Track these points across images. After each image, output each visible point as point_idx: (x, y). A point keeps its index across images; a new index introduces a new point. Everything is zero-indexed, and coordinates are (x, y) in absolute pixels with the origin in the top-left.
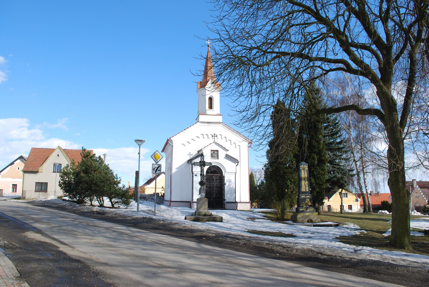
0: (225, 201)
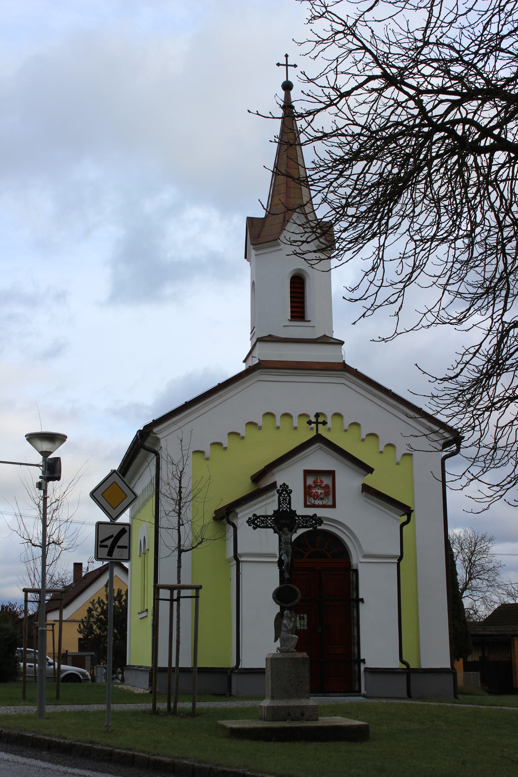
0: (363, 667)
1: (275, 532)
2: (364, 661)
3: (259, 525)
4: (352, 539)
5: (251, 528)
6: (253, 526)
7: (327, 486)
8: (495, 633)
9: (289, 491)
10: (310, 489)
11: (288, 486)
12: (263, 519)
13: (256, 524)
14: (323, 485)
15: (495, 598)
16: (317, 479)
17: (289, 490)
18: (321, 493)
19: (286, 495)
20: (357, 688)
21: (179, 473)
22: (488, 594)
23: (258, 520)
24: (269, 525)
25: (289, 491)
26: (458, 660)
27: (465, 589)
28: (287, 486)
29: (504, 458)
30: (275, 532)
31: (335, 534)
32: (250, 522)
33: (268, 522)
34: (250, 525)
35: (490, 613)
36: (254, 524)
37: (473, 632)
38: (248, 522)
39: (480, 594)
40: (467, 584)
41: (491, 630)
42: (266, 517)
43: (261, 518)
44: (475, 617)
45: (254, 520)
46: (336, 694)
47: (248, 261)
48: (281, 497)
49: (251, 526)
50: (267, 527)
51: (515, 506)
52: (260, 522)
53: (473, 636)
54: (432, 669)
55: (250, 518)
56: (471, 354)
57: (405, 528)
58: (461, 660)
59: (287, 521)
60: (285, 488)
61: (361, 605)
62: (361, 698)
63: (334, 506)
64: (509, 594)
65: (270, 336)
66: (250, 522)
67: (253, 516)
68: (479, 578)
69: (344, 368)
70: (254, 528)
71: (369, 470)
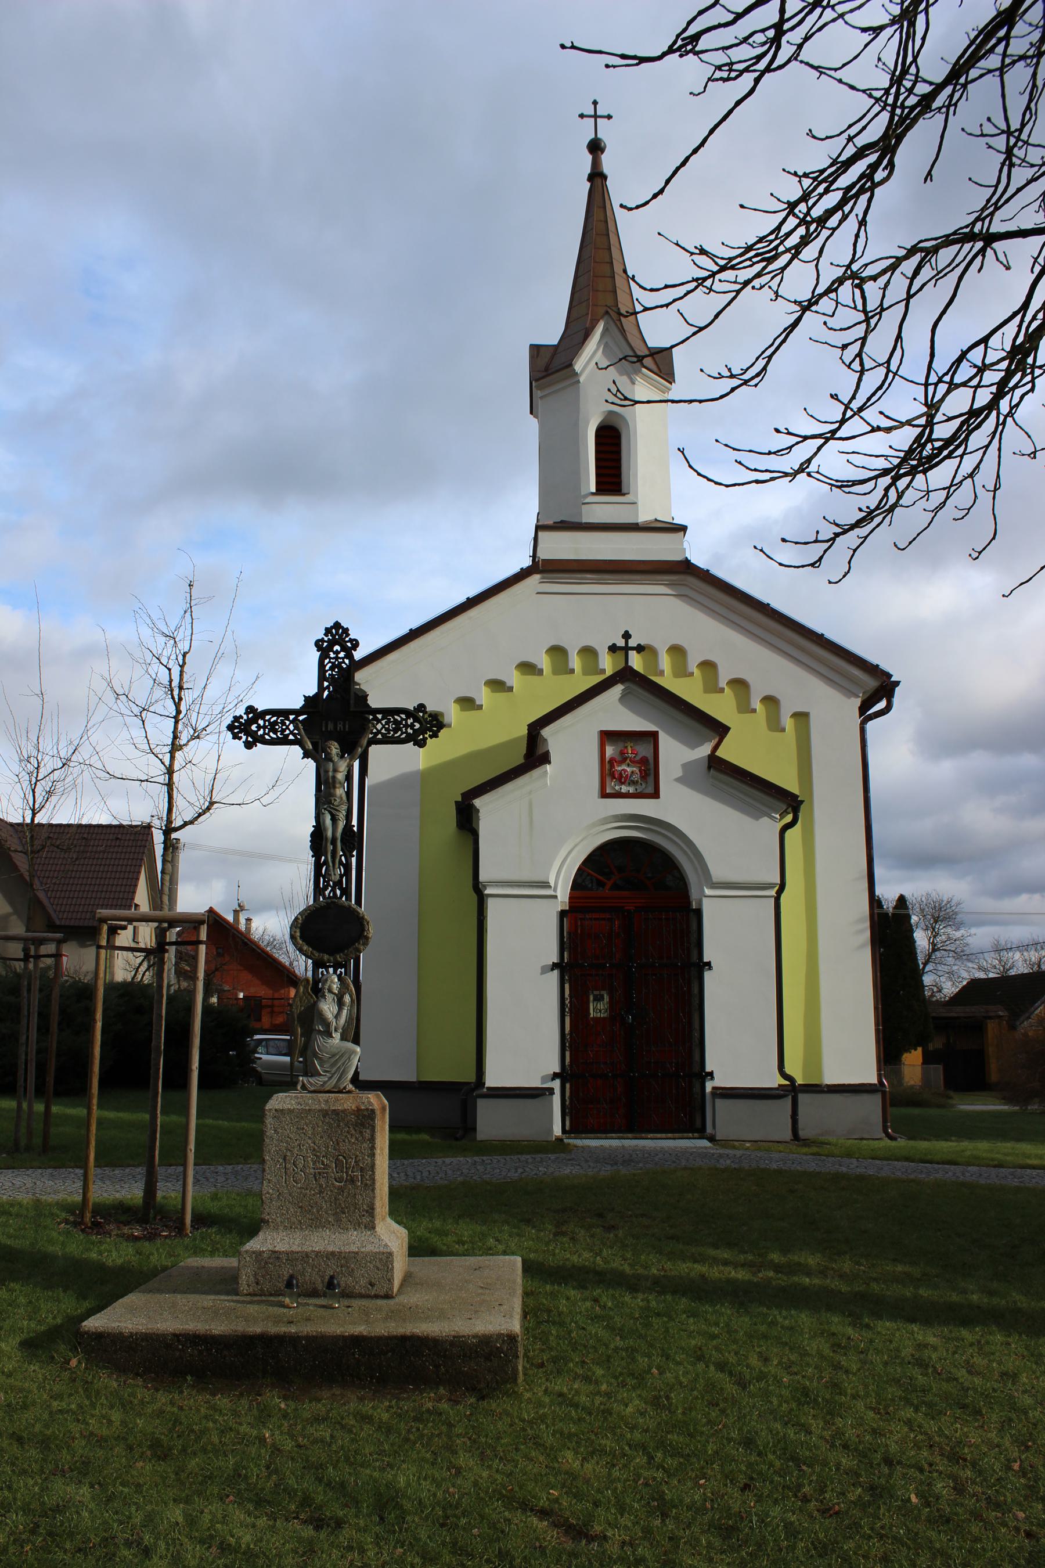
0: (709, 1086)
1: (306, 755)
2: (711, 1074)
3: (262, 736)
4: (689, 853)
5: (239, 744)
6: (244, 738)
7: (644, 761)
8: (962, 1015)
9: (349, 644)
10: (612, 766)
11: (347, 629)
12: (275, 718)
13: (253, 734)
14: (638, 758)
15: (965, 975)
16: (626, 747)
17: (351, 641)
18: (632, 772)
19: (342, 655)
20: (698, 1123)
21: (180, 658)
22: (955, 968)
23: (261, 722)
24: (291, 737)
25: (349, 644)
26: (916, 1050)
27: (925, 964)
28: (346, 631)
29: (961, 482)
30: (306, 755)
31: (660, 845)
32: (237, 727)
33: (287, 728)
34: (235, 737)
35: (957, 990)
36: (248, 732)
37: (934, 1014)
38: (230, 728)
39: (946, 968)
40: (930, 956)
41: (958, 1011)
42: (284, 713)
43: (267, 717)
44: (938, 996)
45: (250, 722)
46: (659, 1135)
47: (536, 417)
48: (327, 661)
49: (240, 738)
50: (284, 741)
51: (994, 538)
52: (264, 727)
53: (934, 1018)
54: (844, 1085)
55: (237, 719)
56: (882, 365)
57: (789, 833)
58: (920, 1049)
59: (340, 726)
60: (341, 636)
61: (707, 975)
62: (705, 1143)
63: (656, 795)
64: (981, 968)
65: (562, 522)
66: (237, 727)
67: (247, 713)
68: (945, 950)
69: (686, 567)
70: (249, 746)
71: (721, 730)
